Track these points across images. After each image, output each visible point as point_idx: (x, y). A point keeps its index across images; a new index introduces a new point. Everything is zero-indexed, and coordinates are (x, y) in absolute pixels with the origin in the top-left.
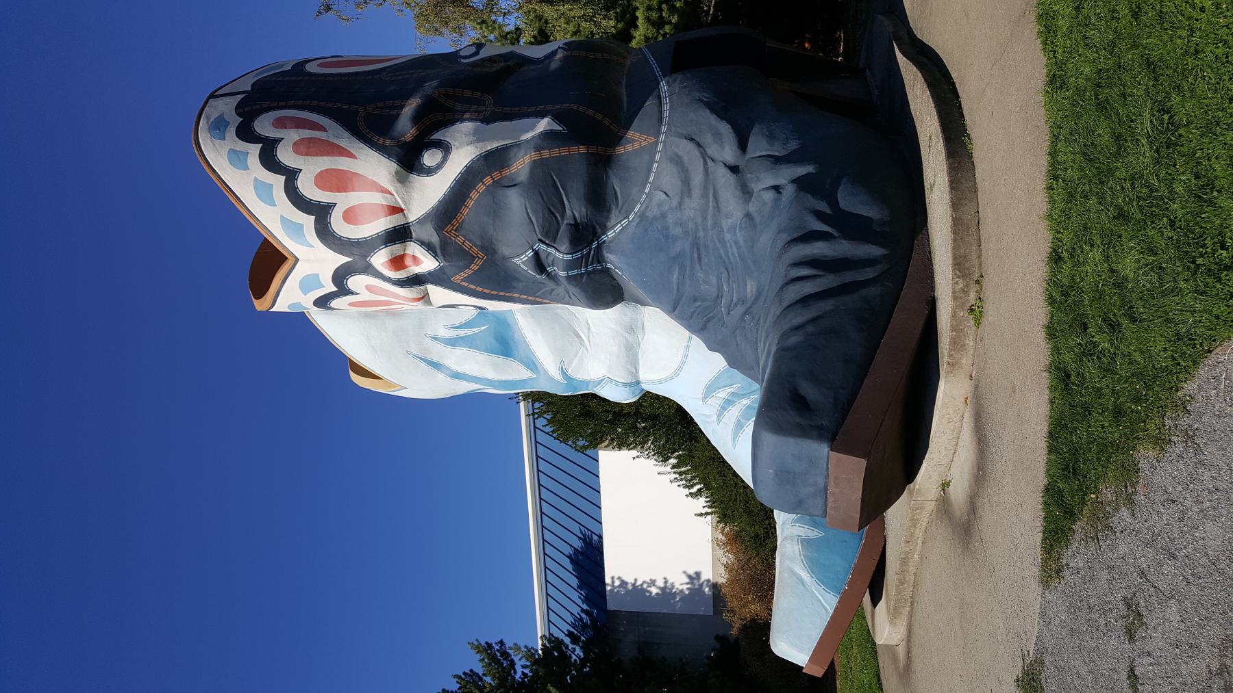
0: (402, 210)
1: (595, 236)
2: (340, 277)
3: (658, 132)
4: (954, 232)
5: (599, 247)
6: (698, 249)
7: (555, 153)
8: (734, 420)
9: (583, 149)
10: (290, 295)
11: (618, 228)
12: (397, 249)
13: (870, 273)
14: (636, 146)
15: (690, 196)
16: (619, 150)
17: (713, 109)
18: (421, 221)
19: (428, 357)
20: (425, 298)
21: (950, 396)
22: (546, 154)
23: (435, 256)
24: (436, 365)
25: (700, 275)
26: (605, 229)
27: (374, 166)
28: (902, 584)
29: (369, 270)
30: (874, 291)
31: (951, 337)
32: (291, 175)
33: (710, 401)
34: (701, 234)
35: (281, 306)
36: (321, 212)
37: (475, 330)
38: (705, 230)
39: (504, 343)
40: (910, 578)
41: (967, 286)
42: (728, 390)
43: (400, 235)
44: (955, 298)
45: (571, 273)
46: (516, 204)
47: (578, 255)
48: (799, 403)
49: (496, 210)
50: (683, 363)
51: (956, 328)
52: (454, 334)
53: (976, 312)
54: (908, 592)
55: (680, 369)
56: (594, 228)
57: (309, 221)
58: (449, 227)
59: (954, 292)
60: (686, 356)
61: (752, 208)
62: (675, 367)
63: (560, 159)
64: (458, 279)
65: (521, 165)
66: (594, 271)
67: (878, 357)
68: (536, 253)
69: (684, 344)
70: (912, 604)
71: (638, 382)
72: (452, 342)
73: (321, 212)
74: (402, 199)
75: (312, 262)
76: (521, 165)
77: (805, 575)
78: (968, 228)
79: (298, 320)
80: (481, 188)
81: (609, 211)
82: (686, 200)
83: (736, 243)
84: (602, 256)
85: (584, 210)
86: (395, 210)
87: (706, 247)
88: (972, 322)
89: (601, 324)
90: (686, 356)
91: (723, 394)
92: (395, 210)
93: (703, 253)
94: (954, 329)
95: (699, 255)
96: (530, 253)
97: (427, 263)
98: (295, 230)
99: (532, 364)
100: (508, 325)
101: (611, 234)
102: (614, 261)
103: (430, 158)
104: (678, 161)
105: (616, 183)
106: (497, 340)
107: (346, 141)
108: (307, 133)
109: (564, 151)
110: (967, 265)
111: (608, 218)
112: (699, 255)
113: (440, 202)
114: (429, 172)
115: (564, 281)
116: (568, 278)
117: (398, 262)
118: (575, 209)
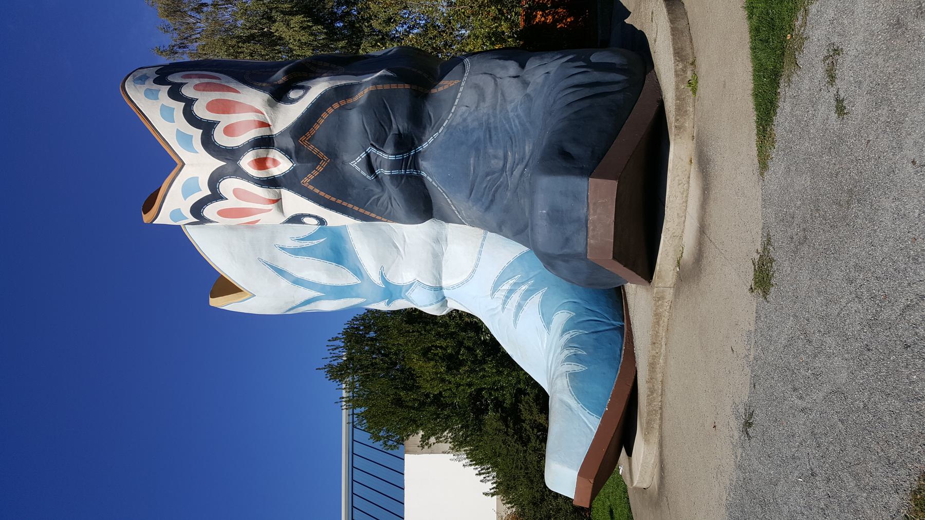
0: (269, 126)
1: (413, 146)
2: (214, 181)
3: (463, 77)
4: (673, 35)
5: (416, 155)
6: (490, 131)
7: (387, 87)
8: (515, 304)
9: (407, 86)
10: (173, 207)
11: (431, 140)
12: (261, 152)
13: (616, 88)
14: (446, 87)
15: (484, 101)
16: (434, 91)
17: (500, 59)
18: (282, 133)
19: (275, 264)
20: (278, 201)
21: (679, 154)
22: (380, 87)
23: (291, 158)
24: (281, 272)
25: (491, 151)
26: (421, 142)
27: (254, 99)
28: (652, 393)
29: (240, 173)
30: (620, 97)
31: (676, 105)
32: (189, 103)
33: (497, 294)
34: (492, 120)
35: (164, 218)
36: (207, 128)
37: (315, 242)
38: (495, 116)
39: (337, 252)
40: (658, 386)
41: (685, 67)
42: (511, 282)
43: (265, 142)
44: (677, 75)
45: (395, 172)
46: (355, 120)
47: (399, 157)
48: (565, 155)
49: (340, 126)
50: (476, 266)
51: (679, 97)
52: (298, 244)
53: (693, 85)
54: (657, 403)
55: (474, 271)
56: (413, 139)
57: (197, 133)
58: (303, 138)
59: (676, 71)
60: (479, 259)
61: (529, 90)
62: (471, 270)
63: (390, 90)
64: (305, 181)
65: (361, 96)
66: (411, 176)
67: (624, 128)
68: (368, 156)
69: (478, 250)
70: (661, 414)
71: (441, 288)
72: (296, 252)
73: (207, 128)
74: (270, 118)
75: (197, 165)
76: (361, 96)
77: (573, 403)
78: (682, 33)
79: (176, 233)
80: (330, 110)
81: (425, 128)
82: (482, 104)
83: (518, 116)
84: (418, 163)
85: (406, 125)
86: (264, 124)
87: (496, 128)
88: (691, 93)
89: (414, 235)
90: (479, 259)
91: (506, 286)
92: (264, 124)
93: (493, 133)
94: (678, 98)
95: (490, 136)
96: (363, 155)
97: (282, 165)
98: (185, 140)
99: (358, 271)
100: (342, 238)
101: (425, 145)
102: (428, 170)
103: (293, 95)
104: (477, 87)
105: (430, 109)
106: (331, 249)
107: (234, 84)
108: (206, 80)
109: (394, 86)
110: (684, 54)
111: (423, 133)
112: (490, 136)
113: (299, 119)
114: (293, 101)
115: (387, 181)
116: (391, 176)
117: (261, 163)
118: (399, 124)
